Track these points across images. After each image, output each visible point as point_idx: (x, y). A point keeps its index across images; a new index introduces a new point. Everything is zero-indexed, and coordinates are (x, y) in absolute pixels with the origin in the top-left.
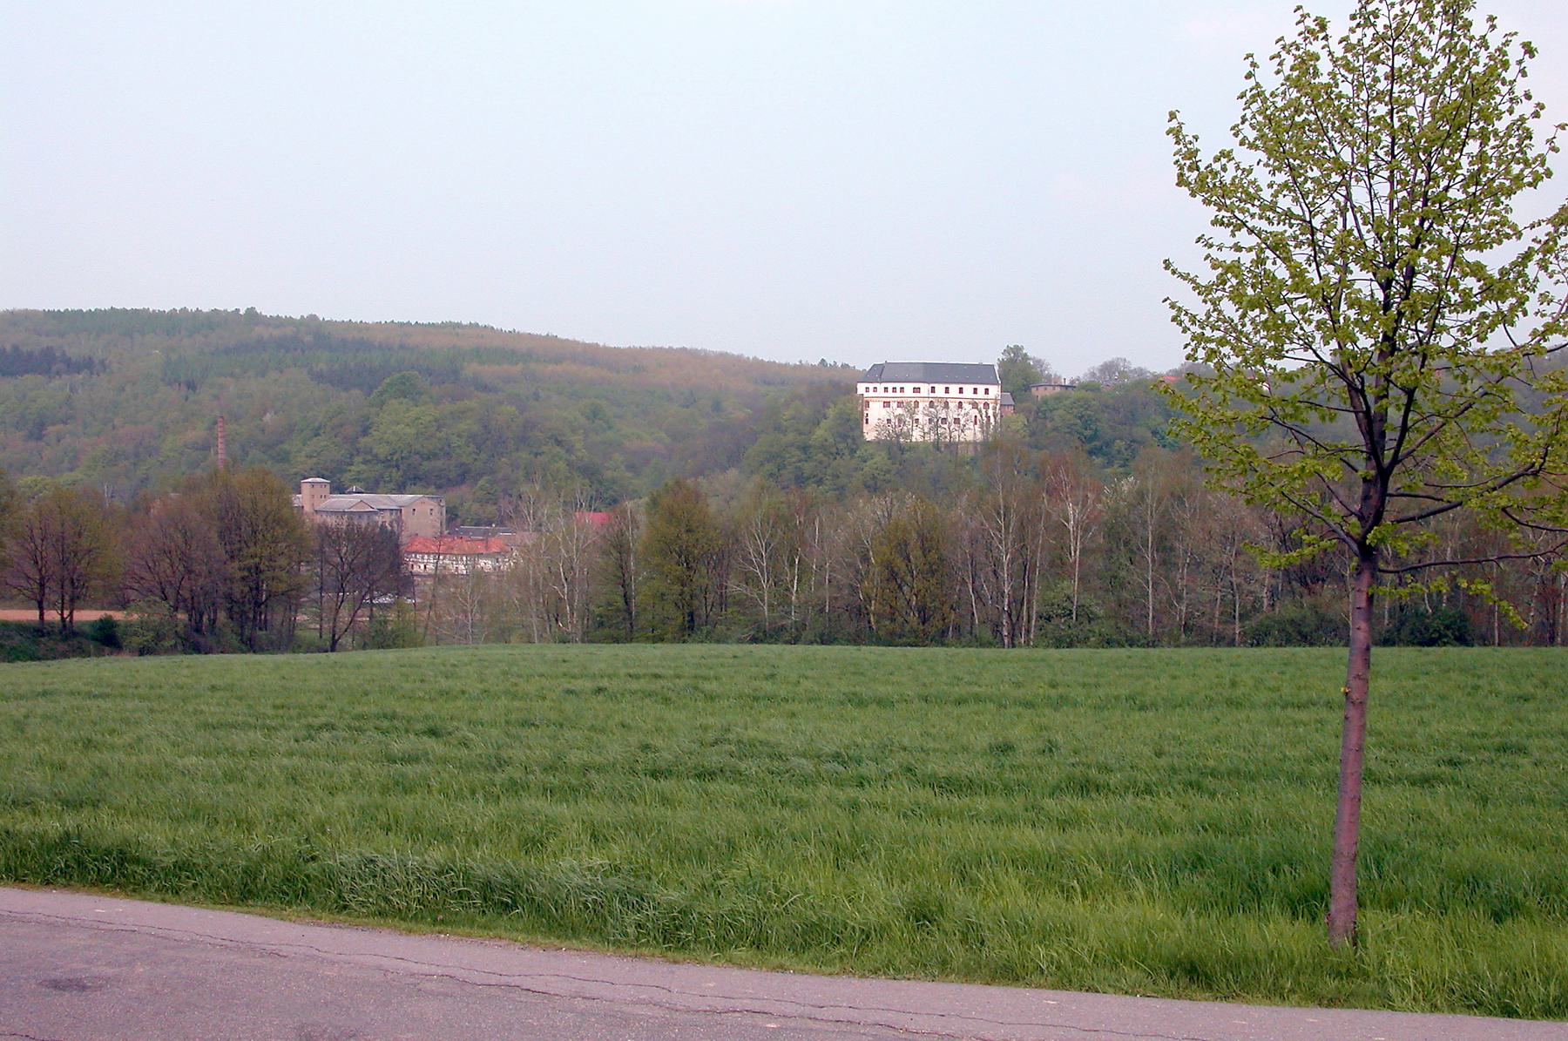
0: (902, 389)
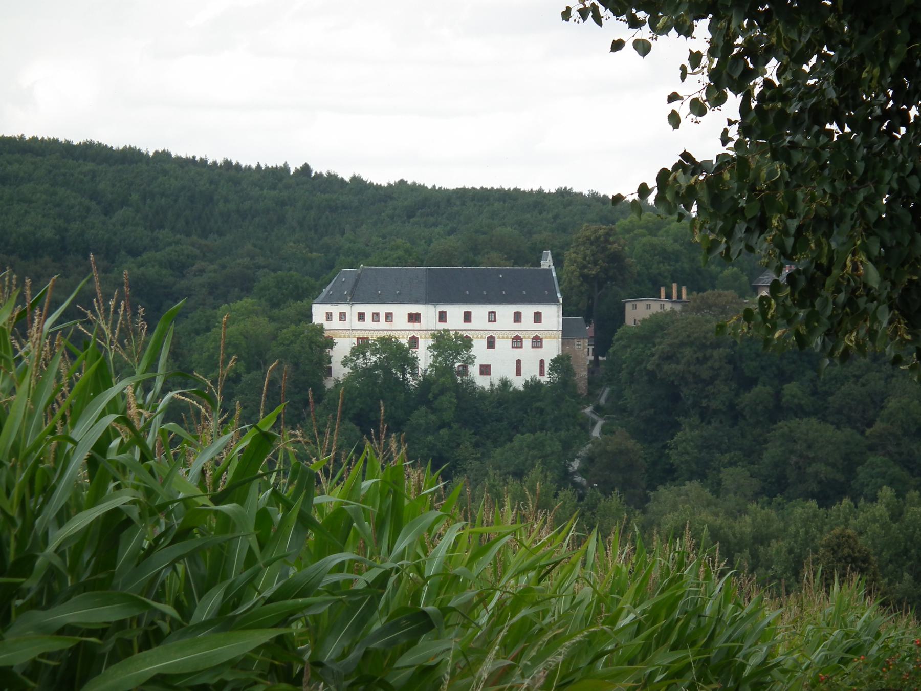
0: (389, 316)
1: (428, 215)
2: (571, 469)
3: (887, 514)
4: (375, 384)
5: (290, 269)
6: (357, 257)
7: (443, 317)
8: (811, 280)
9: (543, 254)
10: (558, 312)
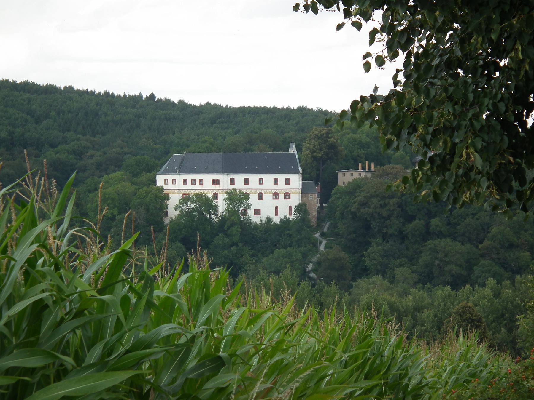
0: (201, 181)
1: (223, 123)
2: (307, 269)
3: (492, 294)
4: (193, 221)
5: (144, 154)
6: (182, 147)
7: (232, 181)
8: (443, 160)
10: (299, 178)
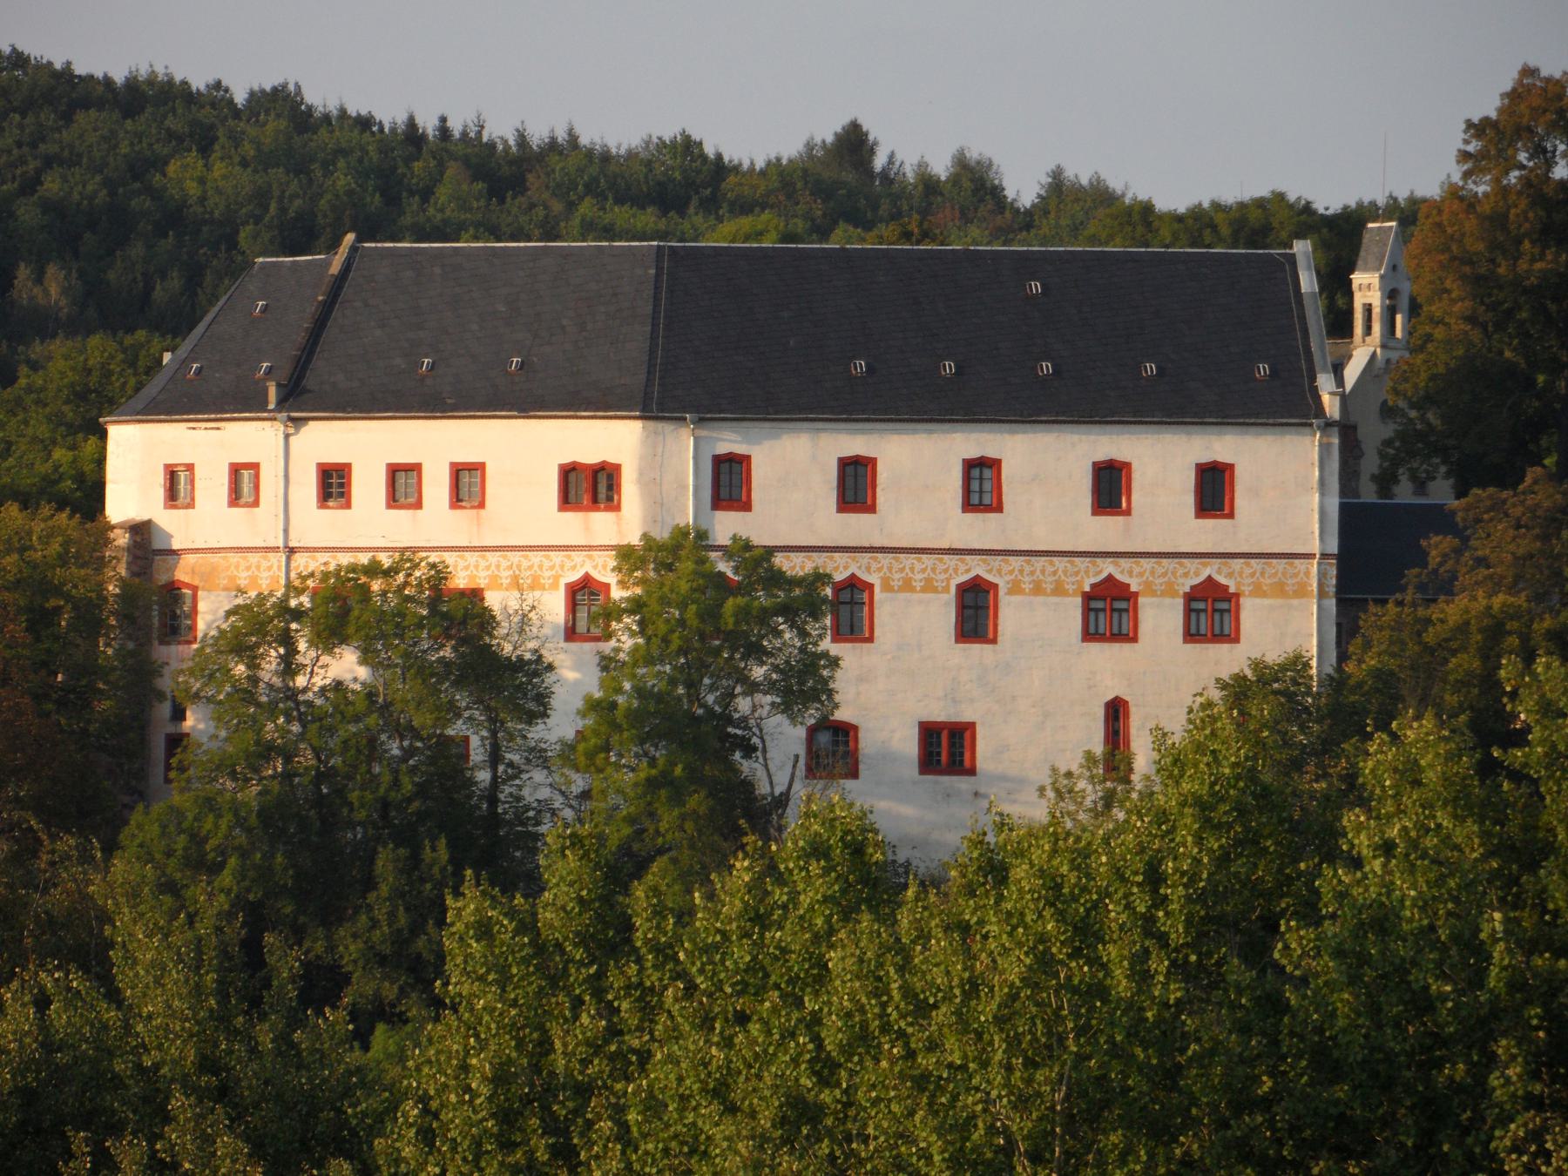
9: (1366, 238)
